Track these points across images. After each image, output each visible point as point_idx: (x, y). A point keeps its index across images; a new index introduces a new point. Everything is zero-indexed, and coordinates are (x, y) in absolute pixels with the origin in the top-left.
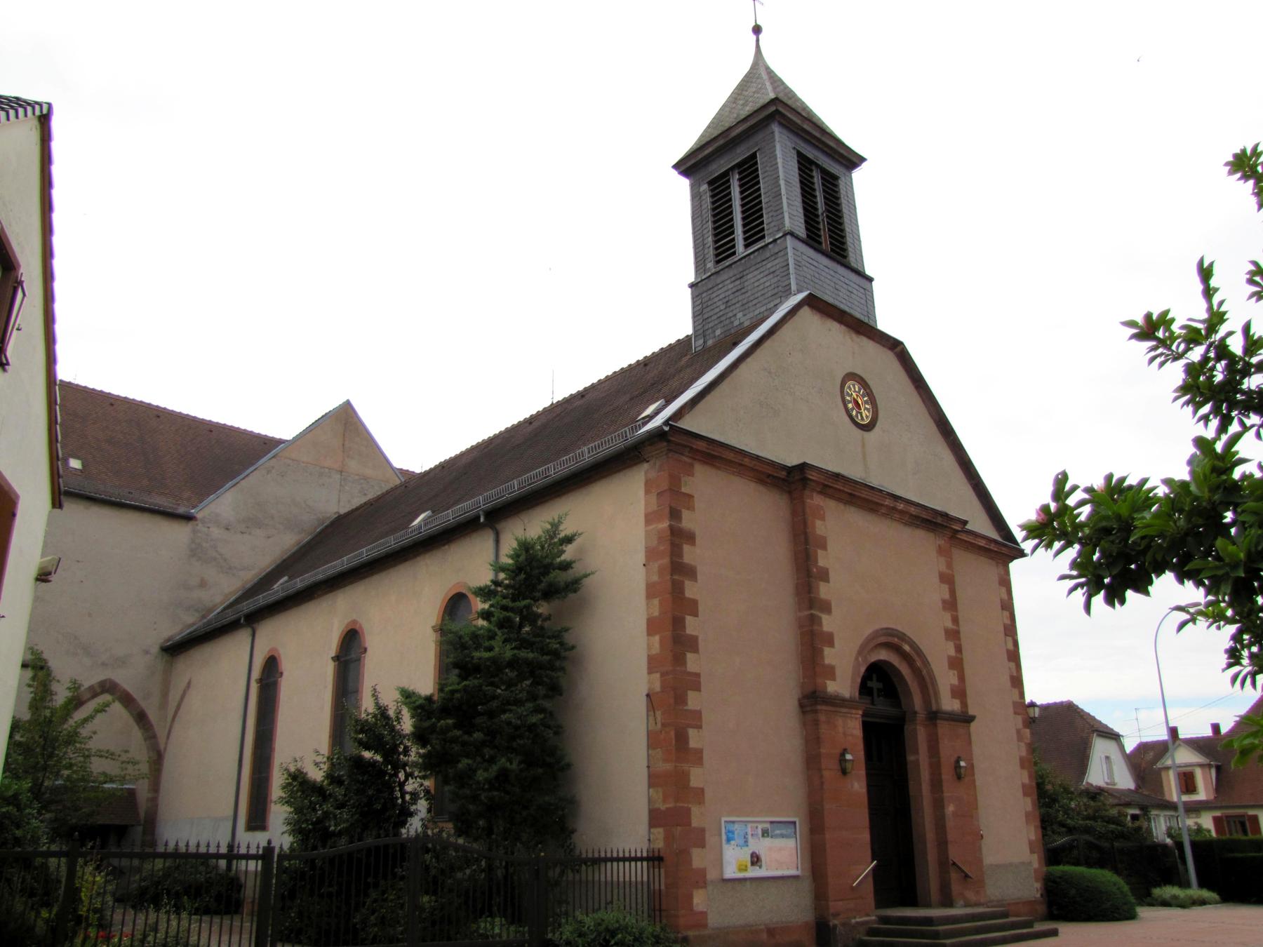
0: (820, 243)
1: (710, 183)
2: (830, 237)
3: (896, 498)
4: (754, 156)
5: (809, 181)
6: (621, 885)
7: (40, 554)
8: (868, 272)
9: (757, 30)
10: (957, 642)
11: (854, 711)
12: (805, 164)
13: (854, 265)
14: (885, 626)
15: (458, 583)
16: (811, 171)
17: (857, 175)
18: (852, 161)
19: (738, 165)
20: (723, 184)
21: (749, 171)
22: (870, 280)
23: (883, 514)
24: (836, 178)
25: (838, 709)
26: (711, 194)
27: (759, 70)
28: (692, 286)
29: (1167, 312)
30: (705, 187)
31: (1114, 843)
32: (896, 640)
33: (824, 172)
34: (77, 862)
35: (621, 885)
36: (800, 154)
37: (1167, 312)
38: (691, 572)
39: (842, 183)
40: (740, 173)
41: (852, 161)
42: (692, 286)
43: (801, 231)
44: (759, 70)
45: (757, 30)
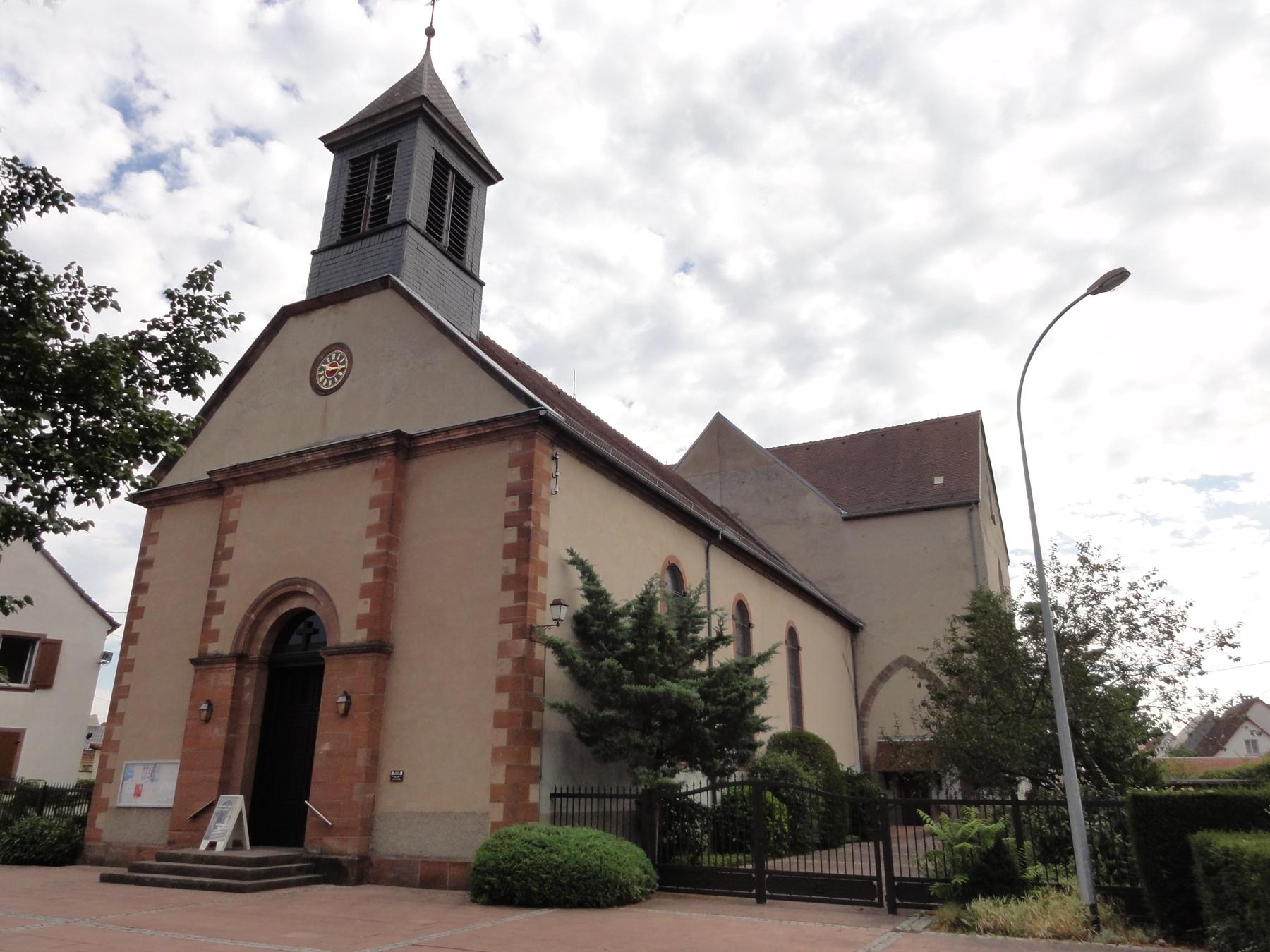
0: (440, 240)
1: (352, 161)
2: (450, 236)
3: (298, 454)
4: (395, 146)
5: (443, 183)
6: (614, 815)
7: (358, 593)
8: (482, 277)
9: (430, 32)
10: (592, 588)
11: (227, 665)
12: (441, 166)
13: (468, 267)
14: (282, 578)
15: (305, 579)
16: (448, 174)
17: (491, 190)
18: (490, 176)
19: (381, 151)
20: (387, 174)
21: (388, 156)
22: (482, 284)
23: (303, 472)
24: (470, 187)
25: (212, 666)
26: (350, 172)
27: (424, 71)
28: (314, 253)
29: (25, 221)
30: (347, 165)
31: (1123, 683)
32: (299, 586)
33: (459, 178)
34: (731, 854)
35: (614, 815)
36: (437, 155)
37: (25, 221)
38: (509, 551)
39: (475, 192)
40: (379, 159)
41: (490, 176)
42: (314, 253)
43: (422, 225)
44: (424, 71)
45: (430, 32)
